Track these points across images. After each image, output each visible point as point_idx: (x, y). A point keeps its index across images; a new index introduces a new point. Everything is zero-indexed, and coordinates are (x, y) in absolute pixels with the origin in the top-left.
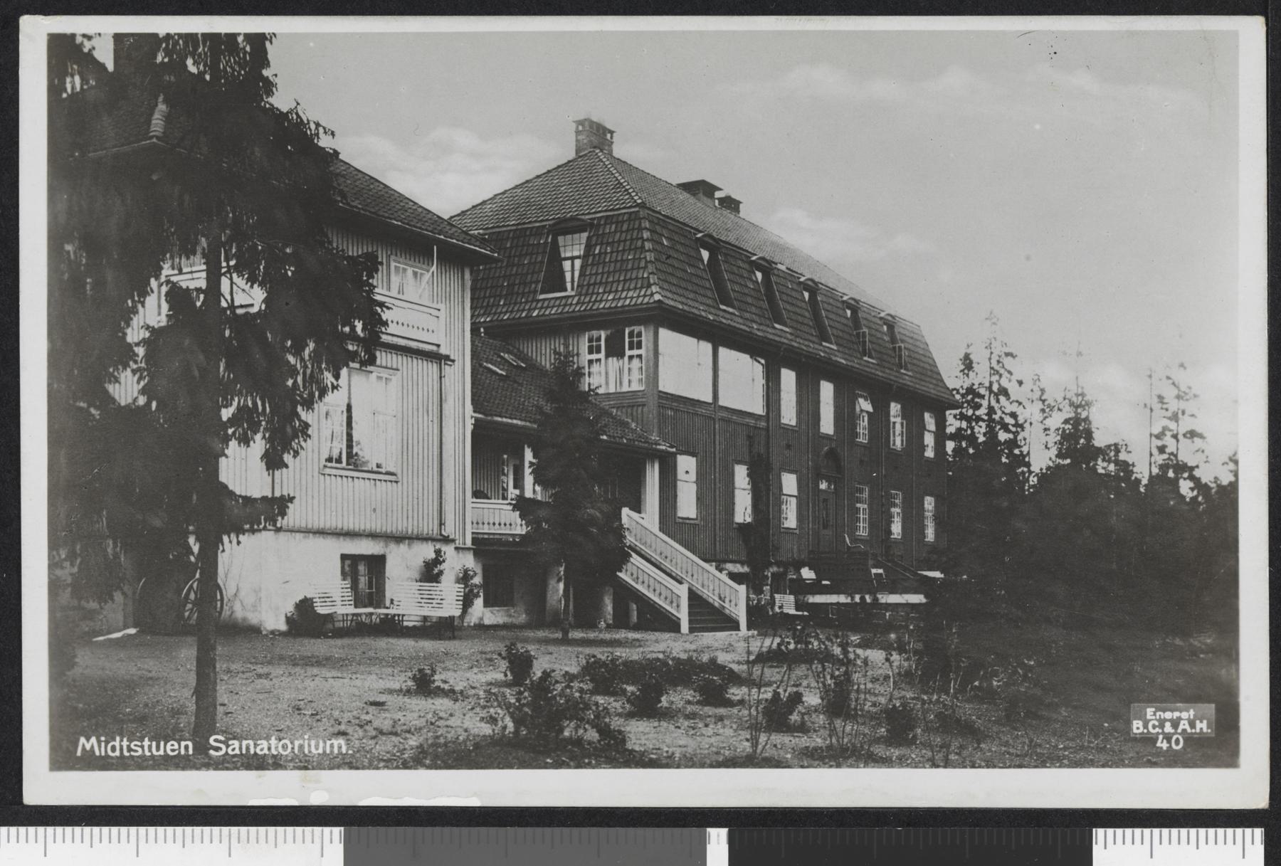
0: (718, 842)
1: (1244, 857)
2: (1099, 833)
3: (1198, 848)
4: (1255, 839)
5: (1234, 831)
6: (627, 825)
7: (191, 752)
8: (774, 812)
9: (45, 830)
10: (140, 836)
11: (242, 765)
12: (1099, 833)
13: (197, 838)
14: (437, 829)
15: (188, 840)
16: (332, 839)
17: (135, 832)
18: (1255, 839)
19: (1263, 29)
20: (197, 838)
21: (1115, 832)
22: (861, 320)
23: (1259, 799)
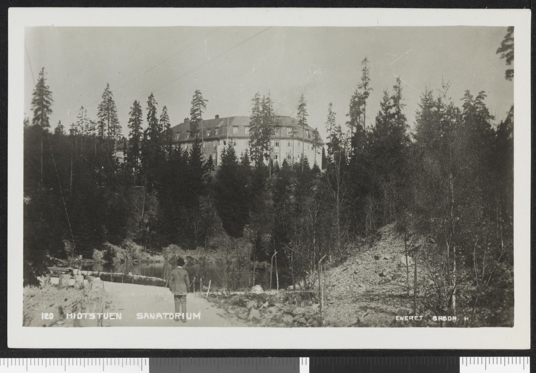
0: (304, 365)
1: (103, 370)
2: (463, 360)
3: (467, 366)
4: (526, 360)
6: (286, 356)
8: (327, 351)
9: (8, 359)
10: (47, 362)
11: (481, 320)
13: (90, 363)
14: (209, 359)
15: (124, 363)
16: (146, 361)
18: (526, 360)
19: (530, 12)
20: (90, 363)
21: (142, 359)
22: (153, 100)
23: (526, 345)
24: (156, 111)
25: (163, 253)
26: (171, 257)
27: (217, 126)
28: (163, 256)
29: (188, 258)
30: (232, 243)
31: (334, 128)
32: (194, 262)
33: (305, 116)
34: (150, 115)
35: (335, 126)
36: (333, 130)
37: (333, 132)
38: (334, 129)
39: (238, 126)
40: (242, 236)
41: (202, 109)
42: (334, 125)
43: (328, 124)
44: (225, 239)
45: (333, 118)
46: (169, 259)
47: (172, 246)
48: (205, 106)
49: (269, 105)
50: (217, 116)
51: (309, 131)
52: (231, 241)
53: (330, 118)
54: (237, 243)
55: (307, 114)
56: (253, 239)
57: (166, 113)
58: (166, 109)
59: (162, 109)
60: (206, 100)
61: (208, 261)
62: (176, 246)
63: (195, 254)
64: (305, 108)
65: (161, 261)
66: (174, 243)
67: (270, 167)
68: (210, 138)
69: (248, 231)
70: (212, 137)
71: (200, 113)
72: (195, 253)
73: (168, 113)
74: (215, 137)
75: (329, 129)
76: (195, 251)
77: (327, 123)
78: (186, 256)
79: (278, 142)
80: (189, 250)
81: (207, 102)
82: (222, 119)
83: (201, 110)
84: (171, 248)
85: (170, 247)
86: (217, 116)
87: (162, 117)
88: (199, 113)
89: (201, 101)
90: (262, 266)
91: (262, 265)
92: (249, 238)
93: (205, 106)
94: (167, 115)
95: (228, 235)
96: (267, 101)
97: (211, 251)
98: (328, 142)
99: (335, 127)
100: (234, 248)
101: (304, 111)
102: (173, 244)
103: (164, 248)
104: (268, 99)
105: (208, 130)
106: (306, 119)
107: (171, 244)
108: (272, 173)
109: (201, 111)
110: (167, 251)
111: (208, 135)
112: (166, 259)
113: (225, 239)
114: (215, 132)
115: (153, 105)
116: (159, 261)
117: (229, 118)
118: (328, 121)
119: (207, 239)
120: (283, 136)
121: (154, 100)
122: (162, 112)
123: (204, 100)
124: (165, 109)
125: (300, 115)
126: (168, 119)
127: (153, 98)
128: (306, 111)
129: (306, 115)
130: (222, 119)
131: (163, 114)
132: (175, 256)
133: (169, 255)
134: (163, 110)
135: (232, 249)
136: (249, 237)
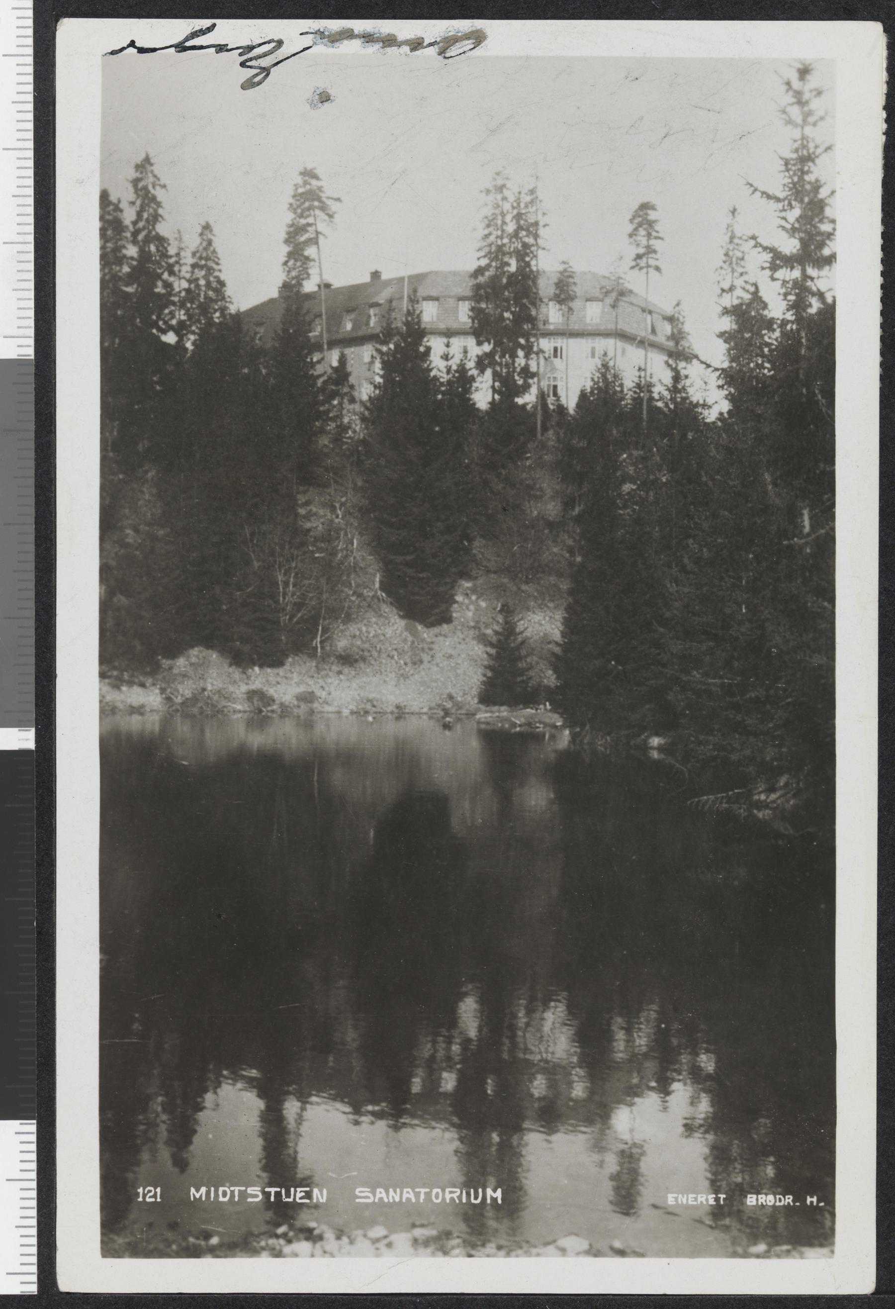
5: (34, 1189)
7: (250, 1200)
12: (31, 1127)
17: (29, 147)
22: (150, 175)
24: (160, 211)
25: (159, 677)
26: (188, 693)
27: (375, 300)
28: (157, 691)
29: (252, 695)
30: (413, 642)
31: (743, 284)
32: (273, 711)
33: (652, 242)
34: (141, 225)
35: (745, 278)
36: (738, 292)
37: (738, 298)
38: (744, 289)
39: (436, 299)
40: (448, 620)
41: (321, 227)
42: (742, 274)
43: (723, 272)
44: (389, 631)
45: (740, 255)
46: (179, 700)
47: (196, 653)
48: (331, 216)
49: (537, 210)
50: (376, 275)
51: (653, 314)
52: (410, 638)
53: (731, 253)
54: (432, 643)
55: (660, 235)
56: (489, 631)
57: (210, 243)
58: (211, 231)
59: (199, 230)
60: (336, 196)
61: (328, 708)
62: (214, 656)
63: (278, 683)
64: (652, 215)
65: (148, 709)
66: (208, 642)
67: (540, 412)
68: (354, 335)
69: (472, 602)
70: (360, 333)
71: (317, 238)
72: (279, 679)
73: (217, 244)
74: (369, 332)
75: (726, 287)
76: (281, 671)
77: (721, 268)
78: (244, 688)
79: (559, 345)
80: (257, 669)
81: (338, 203)
82: (389, 283)
83: (319, 229)
84: (193, 660)
85: (188, 657)
86: (376, 275)
87: (198, 255)
88: (314, 238)
89: (319, 199)
90: (525, 724)
91: (523, 720)
92: (474, 628)
93: (331, 216)
94: (214, 252)
95: (402, 617)
96: (528, 198)
97: (340, 673)
98: (722, 330)
99: (746, 282)
100: (421, 662)
101: (651, 224)
102: (201, 648)
103: (166, 663)
104: (532, 192)
105: (348, 311)
106: (655, 252)
107: (192, 647)
108: (545, 429)
109: (317, 233)
110: (175, 671)
111: (349, 326)
112: (168, 699)
113: (389, 631)
114: (369, 317)
115: (153, 191)
116: (142, 706)
117: (410, 277)
118: (725, 262)
119: (325, 630)
120: (575, 326)
121: (155, 176)
122: (198, 240)
123: (328, 198)
124: (207, 232)
125: (639, 238)
126: (218, 264)
127: (149, 168)
128: (656, 228)
129: (656, 238)
130: (391, 280)
131: (201, 248)
132: (204, 690)
133: (180, 688)
134: (201, 234)
135: (414, 663)
136: (472, 624)
